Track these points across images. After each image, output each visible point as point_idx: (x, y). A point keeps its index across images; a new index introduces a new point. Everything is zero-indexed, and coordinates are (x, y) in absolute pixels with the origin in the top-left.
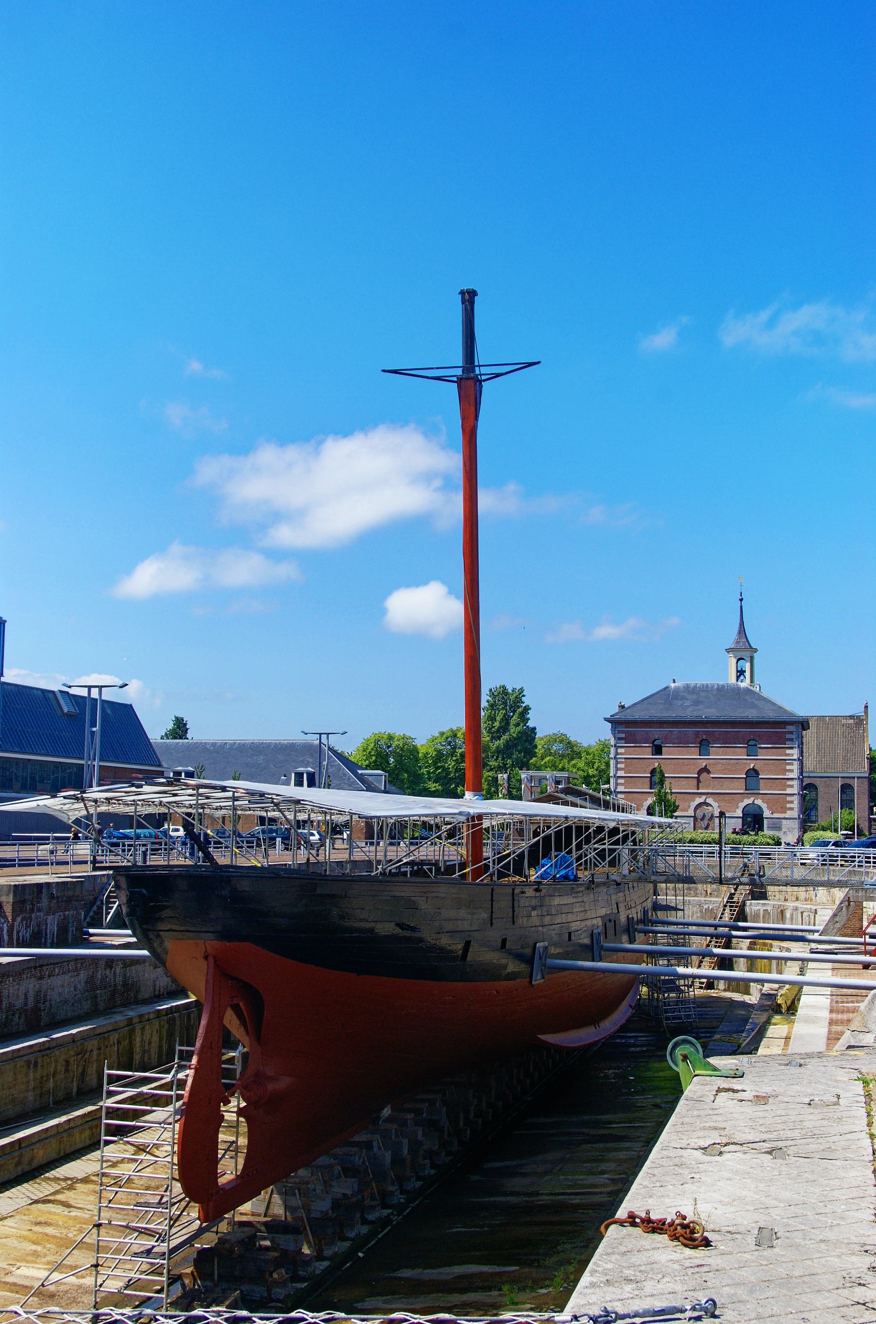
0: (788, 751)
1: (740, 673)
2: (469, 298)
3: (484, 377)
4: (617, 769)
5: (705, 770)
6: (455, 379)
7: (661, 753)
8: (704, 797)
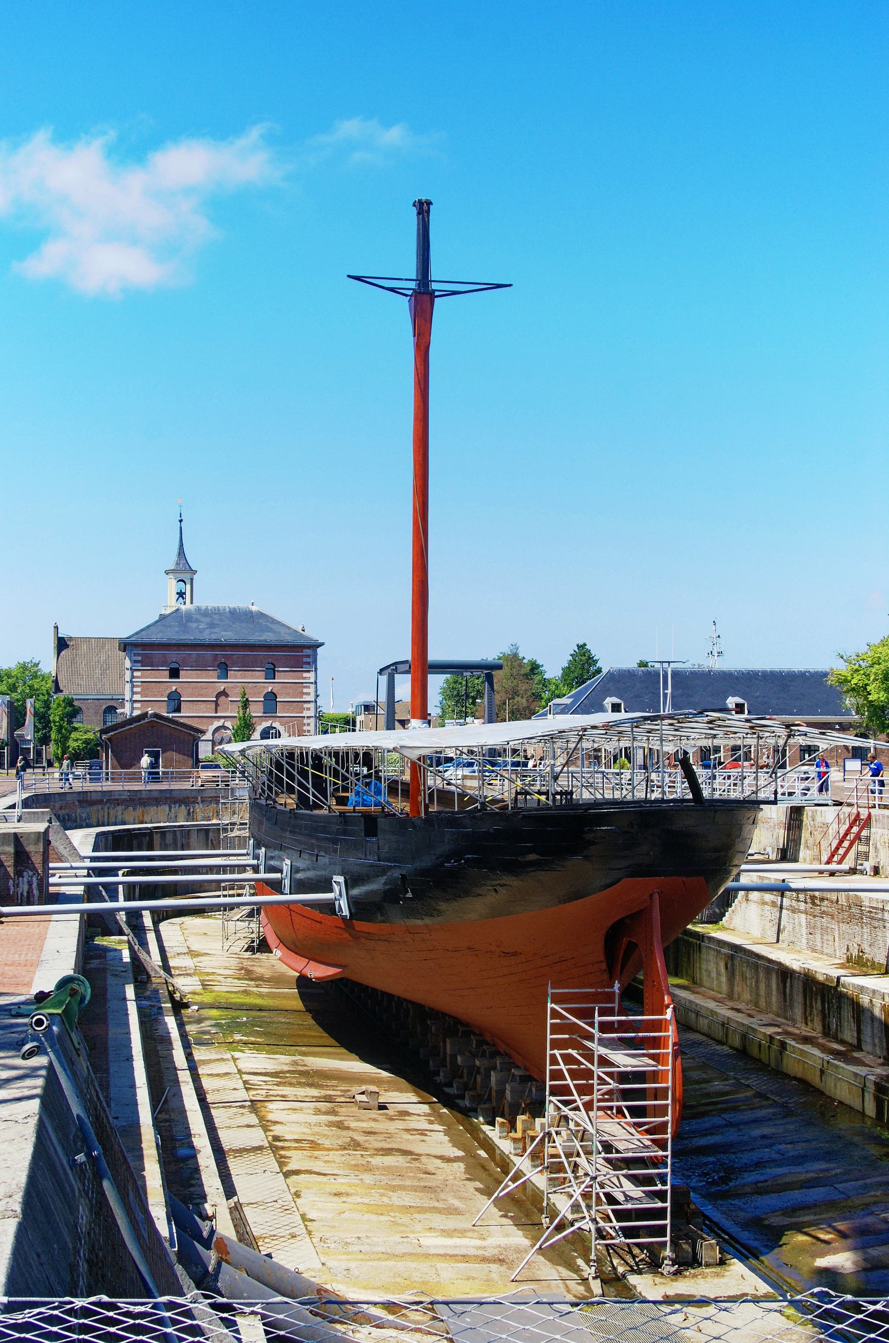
0: (305, 675)
1: (181, 595)
2: (423, 208)
3: (437, 293)
4: (133, 693)
5: (224, 693)
6: (410, 292)
7: (178, 677)
8: (222, 721)
